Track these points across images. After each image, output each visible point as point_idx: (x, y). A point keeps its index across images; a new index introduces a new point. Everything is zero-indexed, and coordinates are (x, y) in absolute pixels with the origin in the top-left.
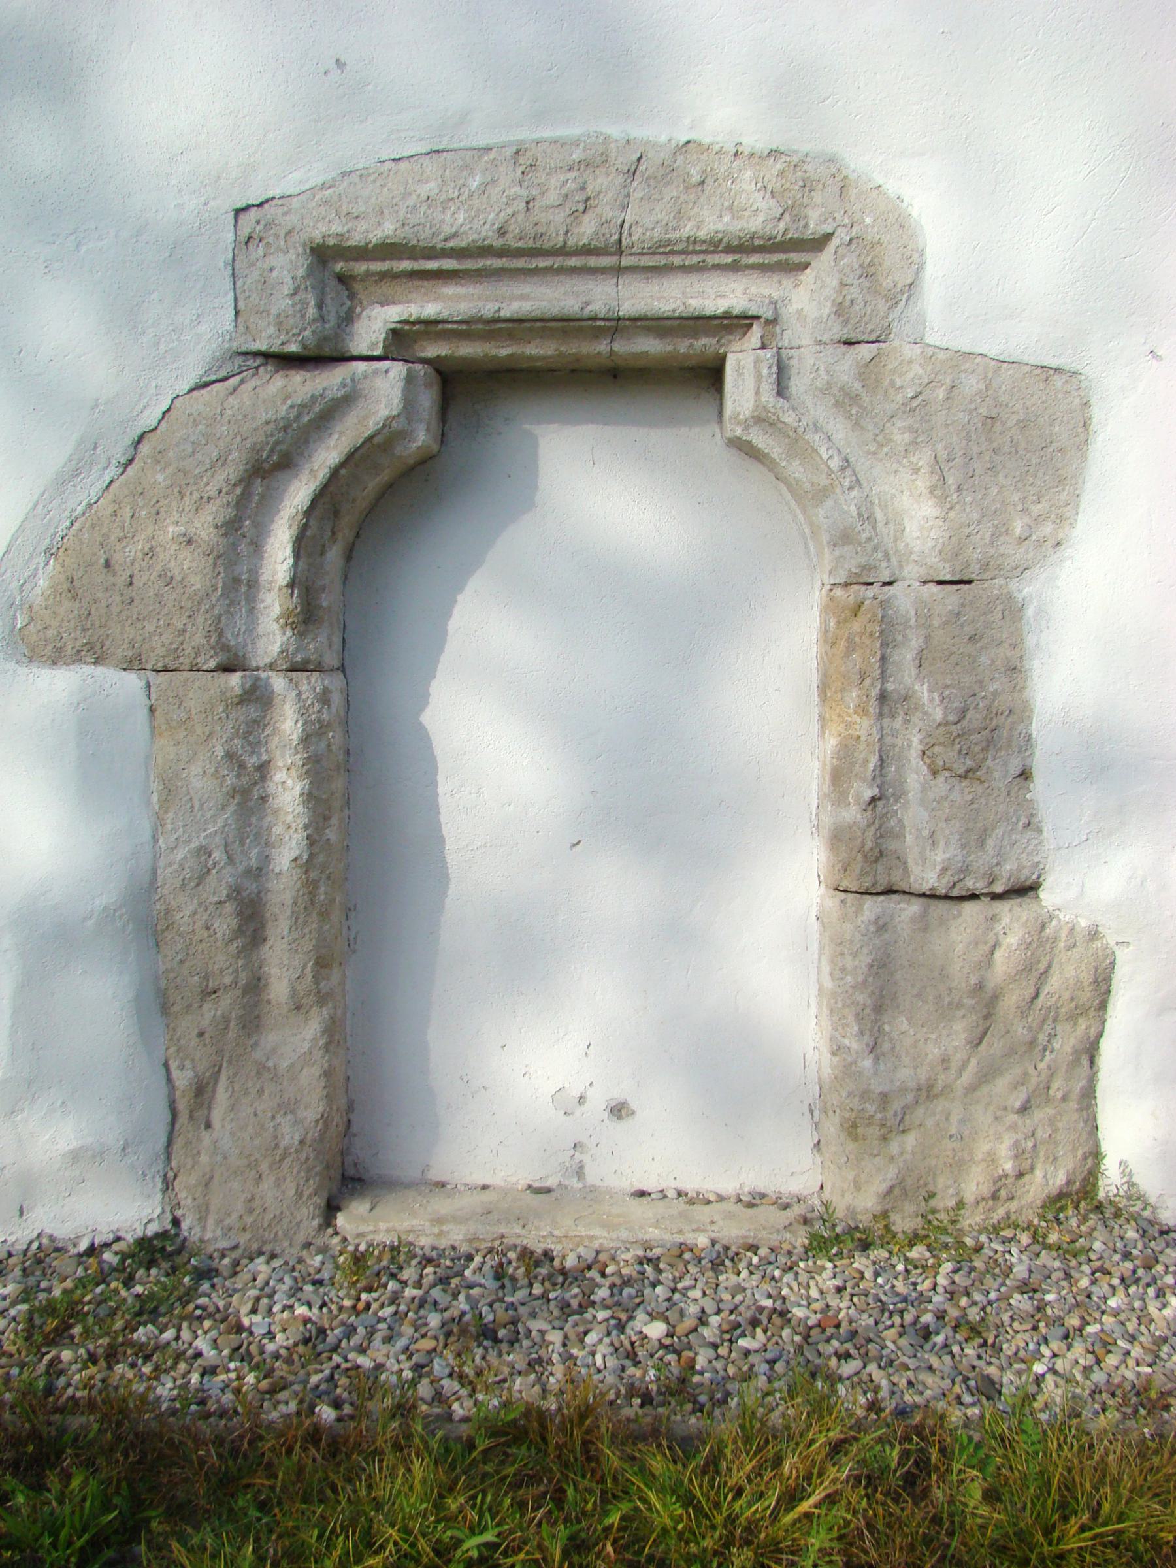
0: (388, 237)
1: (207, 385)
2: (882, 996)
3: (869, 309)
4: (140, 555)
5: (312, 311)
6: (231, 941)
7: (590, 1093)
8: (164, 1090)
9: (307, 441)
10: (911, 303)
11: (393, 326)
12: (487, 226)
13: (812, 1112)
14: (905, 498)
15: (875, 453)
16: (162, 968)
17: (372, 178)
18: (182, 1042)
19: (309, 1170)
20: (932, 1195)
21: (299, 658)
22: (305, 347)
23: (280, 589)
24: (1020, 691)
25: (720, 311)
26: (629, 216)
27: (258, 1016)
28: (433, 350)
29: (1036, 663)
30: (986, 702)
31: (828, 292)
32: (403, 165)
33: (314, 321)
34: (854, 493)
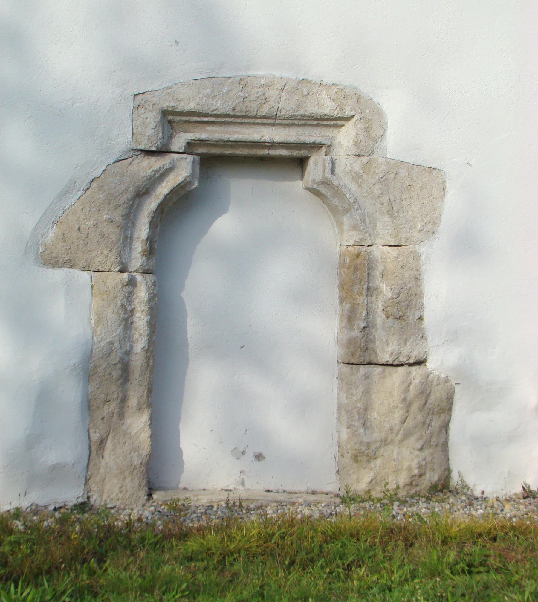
0: (192, 109)
1: (120, 161)
2: (367, 404)
3: (367, 144)
4: (92, 226)
5: (160, 135)
6: (119, 379)
7: (247, 450)
8: (88, 442)
9: (155, 184)
10: (382, 142)
11: (188, 141)
12: (229, 107)
13: (335, 458)
14: (377, 214)
15: (366, 197)
16: (90, 391)
17: (186, 86)
18: (95, 422)
19: (144, 475)
20: (387, 484)
21: (146, 268)
22: (157, 148)
23: (142, 241)
24: (419, 287)
25: (311, 142)
26: (281, 105)
27: (124, 413)
28: (201, 150)
29: (425, 277)
30: (407, 291)
31: (352, 136)
32: (198, 82)
33: (161, 138)
34: (359, 211)
